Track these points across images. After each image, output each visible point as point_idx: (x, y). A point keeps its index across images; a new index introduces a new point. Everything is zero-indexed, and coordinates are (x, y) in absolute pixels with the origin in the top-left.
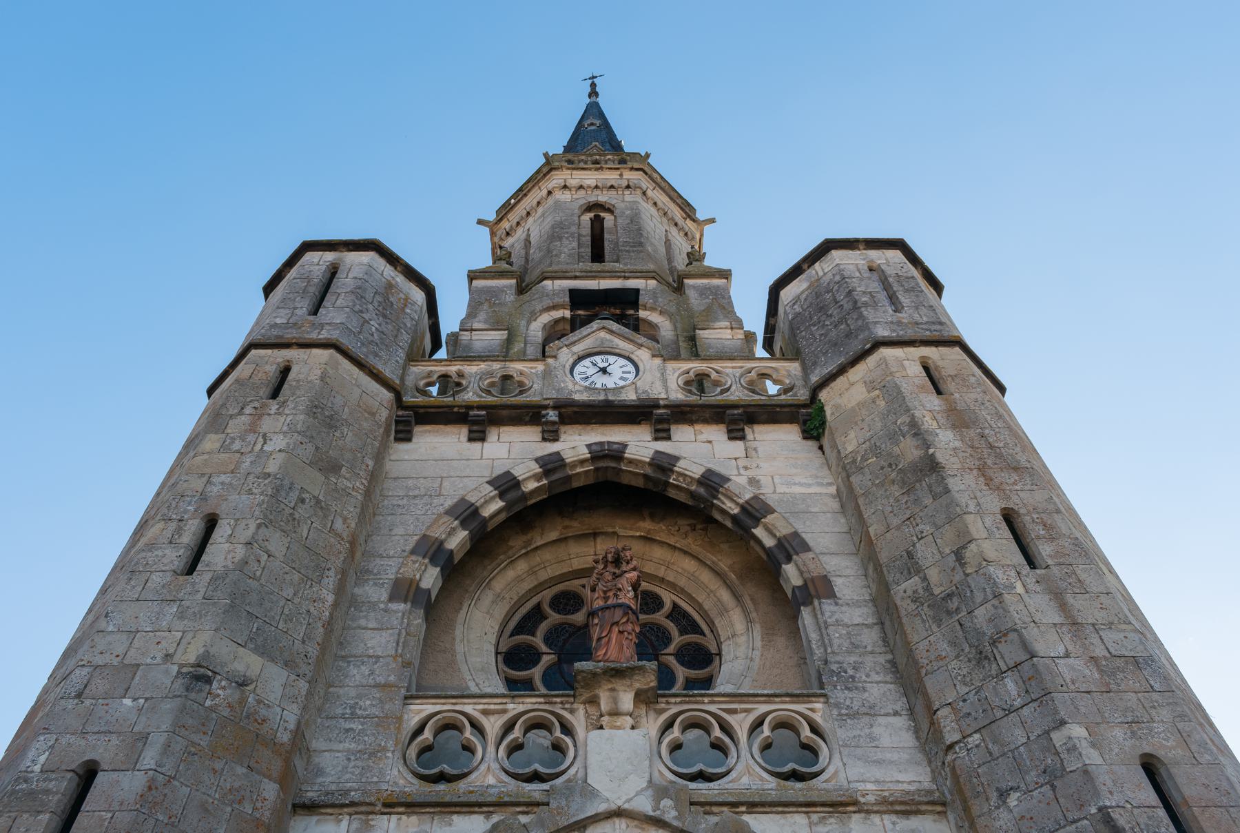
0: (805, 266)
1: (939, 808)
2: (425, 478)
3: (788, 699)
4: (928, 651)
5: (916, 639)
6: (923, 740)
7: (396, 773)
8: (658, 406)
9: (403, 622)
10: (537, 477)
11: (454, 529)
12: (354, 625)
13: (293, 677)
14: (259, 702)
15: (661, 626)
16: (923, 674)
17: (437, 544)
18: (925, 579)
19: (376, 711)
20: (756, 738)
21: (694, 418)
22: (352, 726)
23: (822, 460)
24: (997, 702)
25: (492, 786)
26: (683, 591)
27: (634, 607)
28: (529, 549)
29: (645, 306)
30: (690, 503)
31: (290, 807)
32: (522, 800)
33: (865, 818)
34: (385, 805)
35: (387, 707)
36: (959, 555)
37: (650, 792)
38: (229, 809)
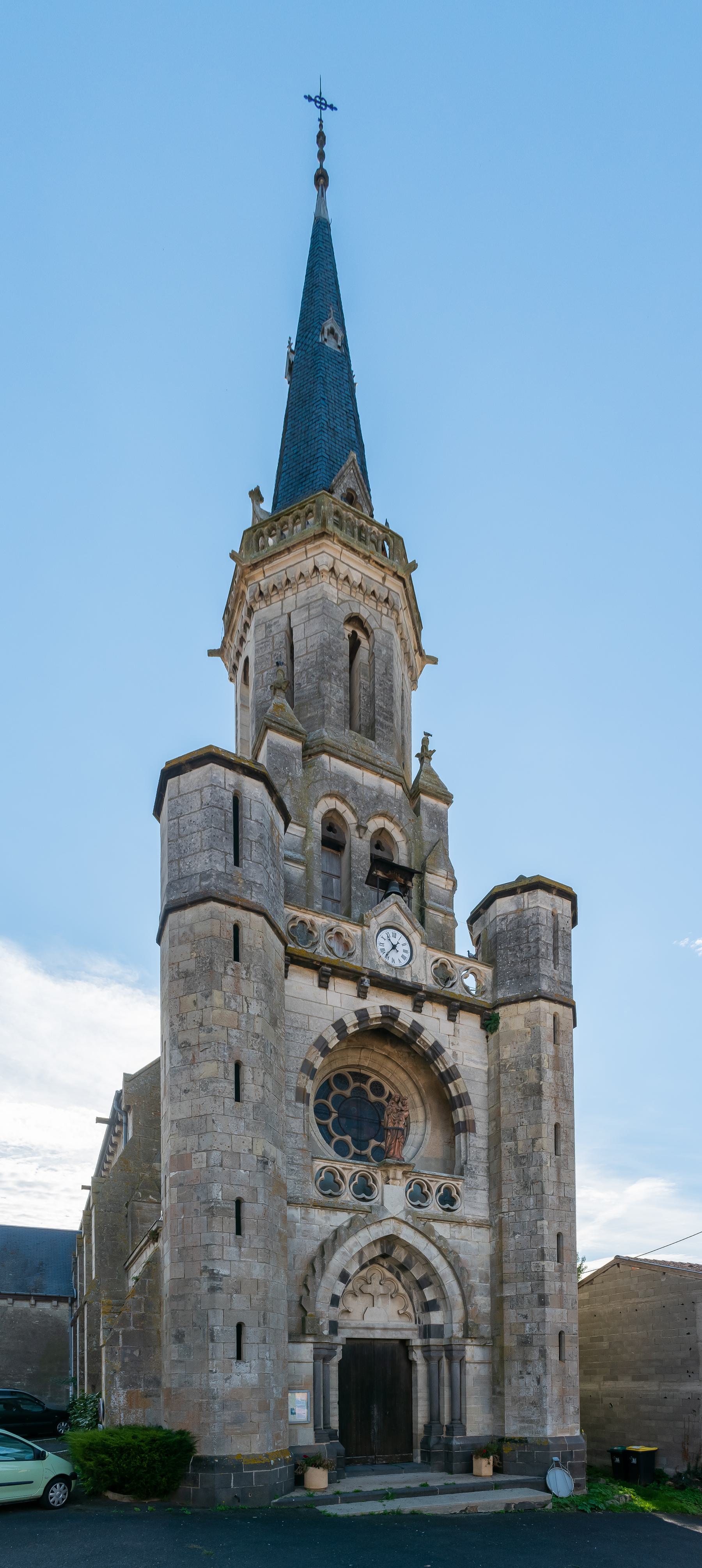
0: (519, 891)
8: (421, 990)
10: (355, 1026)
18: (516, 1145)
23: (484, 1046)
24: (525, 1204)
29: (392, 819)
36: (534, 1141)
37: (404, 1212)
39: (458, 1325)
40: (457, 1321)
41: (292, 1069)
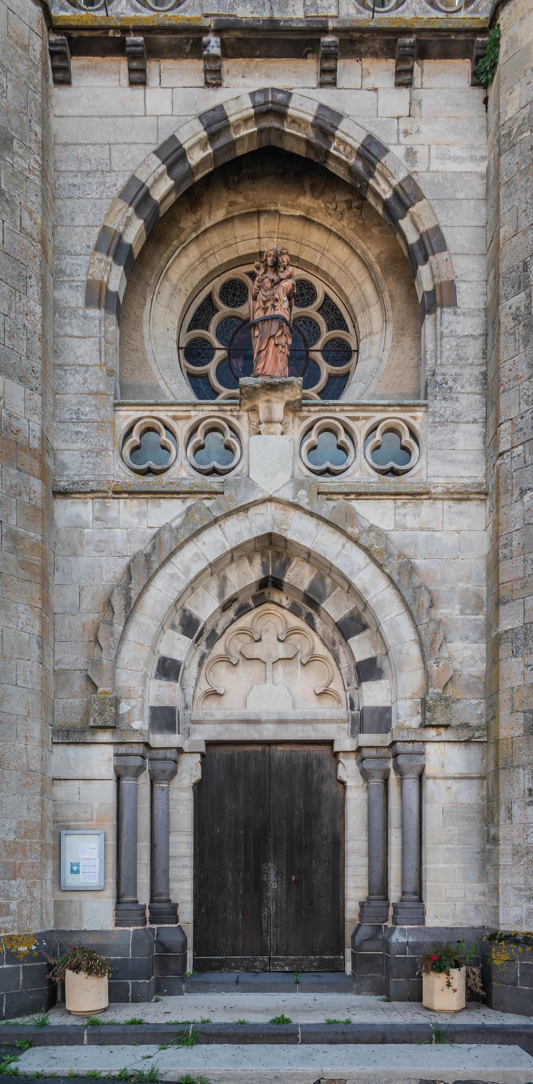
1: (483, 497)
2: (94, 145)
3: (398, 408)
4: (510, 370)
5: (504, 359)
6: (487, 445)
7: (118, 468)
8: (325, 31)
9: (100, 330)
10: (202, 144)
11: (129, 218)
12: (62, 333)
13: (29, 392)
14: (10, 416)
15: (312, 320)
16: (501, 392)
17: (117, 239)
19: (94, 416)
20: (369, 441)
21: (363, 50)
22: (79, 429)
23: (482, 121)
25: (185, 479)
26: (334, 281)
27: (288, 318)
28: (199, 232)
30: (347, 180)
31: (51, 493)
32: (206, 490)
33: (432, 504)
34: (115, 492)
35: (102, 412)
37: (291, 485)
38: (14, 500)
39: (409, 703)
40: (408, 694)
41: (78, 249)
